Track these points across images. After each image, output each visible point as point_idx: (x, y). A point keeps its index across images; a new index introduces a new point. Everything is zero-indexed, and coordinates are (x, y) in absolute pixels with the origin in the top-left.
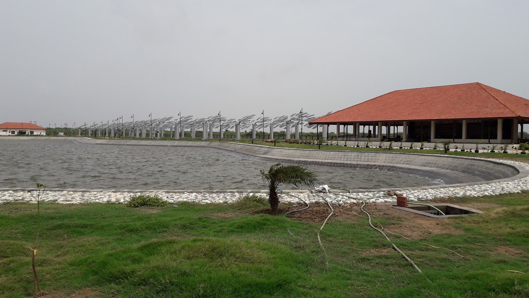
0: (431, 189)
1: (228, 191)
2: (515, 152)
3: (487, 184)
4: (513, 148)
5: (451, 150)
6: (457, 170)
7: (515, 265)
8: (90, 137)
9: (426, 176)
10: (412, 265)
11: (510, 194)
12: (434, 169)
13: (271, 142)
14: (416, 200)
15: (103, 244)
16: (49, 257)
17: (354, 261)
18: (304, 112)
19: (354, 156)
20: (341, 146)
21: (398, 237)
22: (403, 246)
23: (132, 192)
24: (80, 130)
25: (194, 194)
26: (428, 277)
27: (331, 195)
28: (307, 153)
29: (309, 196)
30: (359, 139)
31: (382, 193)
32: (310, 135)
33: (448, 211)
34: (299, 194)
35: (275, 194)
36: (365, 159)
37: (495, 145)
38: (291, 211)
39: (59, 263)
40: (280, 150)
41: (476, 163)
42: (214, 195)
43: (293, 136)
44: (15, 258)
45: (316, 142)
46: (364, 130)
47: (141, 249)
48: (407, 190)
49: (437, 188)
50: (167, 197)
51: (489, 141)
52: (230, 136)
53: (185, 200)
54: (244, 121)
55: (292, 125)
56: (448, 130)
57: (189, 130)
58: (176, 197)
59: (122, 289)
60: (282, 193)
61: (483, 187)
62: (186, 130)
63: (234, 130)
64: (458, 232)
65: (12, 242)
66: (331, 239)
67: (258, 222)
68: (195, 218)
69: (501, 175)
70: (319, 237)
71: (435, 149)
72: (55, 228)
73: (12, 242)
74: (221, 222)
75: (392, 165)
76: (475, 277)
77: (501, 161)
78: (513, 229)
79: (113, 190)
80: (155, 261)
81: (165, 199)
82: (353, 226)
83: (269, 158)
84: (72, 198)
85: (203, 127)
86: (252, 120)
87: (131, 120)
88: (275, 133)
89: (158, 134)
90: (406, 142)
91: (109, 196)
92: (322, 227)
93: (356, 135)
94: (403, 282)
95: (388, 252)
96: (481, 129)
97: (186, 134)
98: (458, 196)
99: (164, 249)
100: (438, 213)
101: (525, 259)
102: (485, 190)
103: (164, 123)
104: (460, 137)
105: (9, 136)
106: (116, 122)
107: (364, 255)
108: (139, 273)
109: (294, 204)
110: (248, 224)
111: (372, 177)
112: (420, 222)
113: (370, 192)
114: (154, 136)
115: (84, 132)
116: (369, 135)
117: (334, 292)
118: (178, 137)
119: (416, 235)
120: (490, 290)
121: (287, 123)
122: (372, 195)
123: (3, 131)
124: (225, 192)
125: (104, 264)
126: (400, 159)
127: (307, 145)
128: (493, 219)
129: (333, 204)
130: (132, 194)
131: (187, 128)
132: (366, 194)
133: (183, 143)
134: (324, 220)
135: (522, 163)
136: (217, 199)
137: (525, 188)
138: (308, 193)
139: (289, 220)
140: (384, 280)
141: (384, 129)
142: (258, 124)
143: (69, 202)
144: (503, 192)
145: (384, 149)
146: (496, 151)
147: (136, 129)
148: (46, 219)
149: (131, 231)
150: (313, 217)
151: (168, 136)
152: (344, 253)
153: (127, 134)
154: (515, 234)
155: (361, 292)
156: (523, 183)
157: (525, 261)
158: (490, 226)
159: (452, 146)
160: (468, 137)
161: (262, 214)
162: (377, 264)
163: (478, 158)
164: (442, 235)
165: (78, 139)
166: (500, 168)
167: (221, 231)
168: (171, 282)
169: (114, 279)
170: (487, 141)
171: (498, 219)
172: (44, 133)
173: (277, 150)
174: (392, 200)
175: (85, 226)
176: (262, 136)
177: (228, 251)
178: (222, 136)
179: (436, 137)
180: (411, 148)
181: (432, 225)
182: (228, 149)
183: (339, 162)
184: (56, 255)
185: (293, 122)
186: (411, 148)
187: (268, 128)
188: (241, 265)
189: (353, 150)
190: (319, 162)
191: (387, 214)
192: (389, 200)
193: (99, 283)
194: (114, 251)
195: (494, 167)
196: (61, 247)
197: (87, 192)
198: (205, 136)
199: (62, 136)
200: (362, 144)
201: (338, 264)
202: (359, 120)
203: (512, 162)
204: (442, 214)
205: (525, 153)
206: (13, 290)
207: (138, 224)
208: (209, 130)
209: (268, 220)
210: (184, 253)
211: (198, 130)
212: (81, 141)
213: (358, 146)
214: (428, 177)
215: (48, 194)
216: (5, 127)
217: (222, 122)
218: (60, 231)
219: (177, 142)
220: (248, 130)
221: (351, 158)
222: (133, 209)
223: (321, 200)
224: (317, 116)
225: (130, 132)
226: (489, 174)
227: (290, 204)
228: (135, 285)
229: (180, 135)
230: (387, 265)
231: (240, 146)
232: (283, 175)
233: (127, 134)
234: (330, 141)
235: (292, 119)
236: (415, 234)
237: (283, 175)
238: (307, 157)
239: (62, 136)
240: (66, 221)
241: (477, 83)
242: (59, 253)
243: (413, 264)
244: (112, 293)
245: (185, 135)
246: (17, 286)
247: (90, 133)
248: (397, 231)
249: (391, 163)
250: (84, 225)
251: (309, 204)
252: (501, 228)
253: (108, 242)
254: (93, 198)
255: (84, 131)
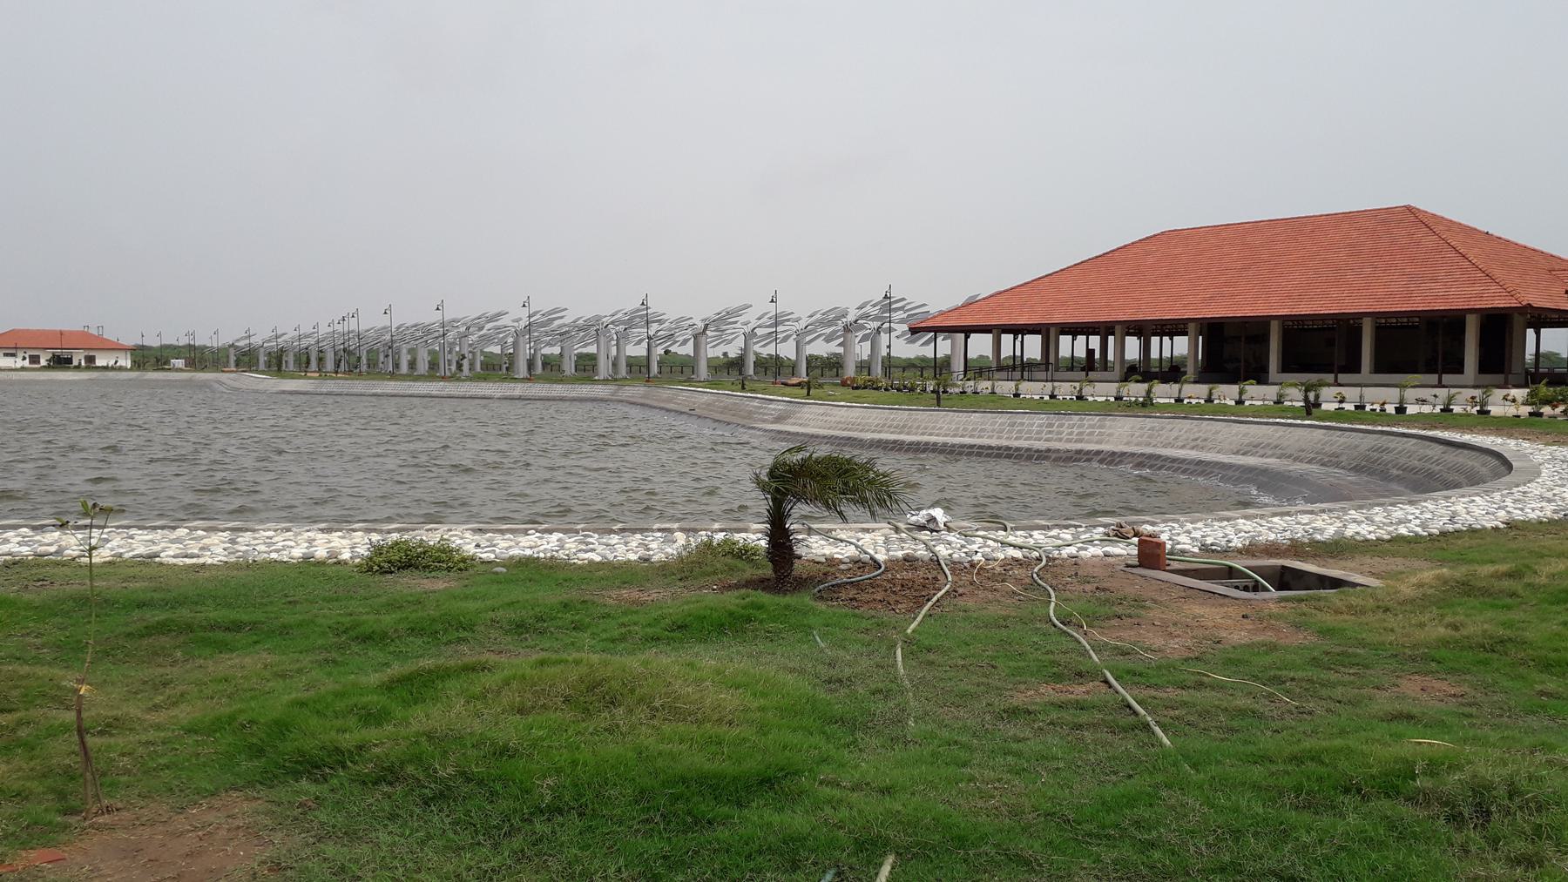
0: (1246, 517)
1: (656, 526)
2: (1511, 411)
3: (1411, 503)
4: (1505, 398)
5: (1324, 406)
6: (1337, 465)
7: (1436, 725)
8: (262, 372)
9: (1248, 481)
10: (1147, 727)
11: (1472, 531)
12: (1272, 462)
13: (799, 385)
14: (1196, 550)
15: (283, 676)
16: (133, 710)
17: (988, 717)
18: (896, 295)
19: (1040, 426)
20: (1003, 398)
21: (1125, 654)
22: (1131, 676)
23: (375, 530)
24: (232, 351)
25: (555, 536)
26: (1186, 757)
27: (951, 537)
28: (900, 416)
29: (887, 540)
30: (1057, 375)
31: (1101, 529)
32: (918, 363)
33: (1285, 579)
34: (860, 535)
35: (786, 533)
36: (1070, 433)
37: (1453, 391)
38: (829, 581)
39: (158, 727)
40: (822, 409)
41: (1394, 443)
42: (614, 539)
43: (864, 366)
44: (34, 713)
45: (930, 387)
46: (1067, 346)
47: (389, 687)
48: (1174, 520)
49: (1262, 517)
50: (478, 546)
51: (1440, 380)
52: (678, 370)
53: (528, 552)
54: (720, 322)
55: (860, 334)
56: (1320, 346)
57: (556, 350)
58: (503, 544)
59: (326, 794)
60: (810, 531)
61: (1398, 513)
62: (547, 351)
63: (688, 350)
64: (1300, 639)
65: (25, 669)
66: (931, 657)
67: (731, 614)
68: (550, 603)
69: (1462, 479)
70: (899, 652)
71: (1278, 402)
72: (151, 630)
73: (25, 669)
74: (625, 613)
75: (1149, 450)
76: (1316, 758)
77: (1467, 438)
78: (1456, 628)
79: (323, 526)
80: (423, 718)
81: (470, 549)
82: (1001, 623)
83: (789, 433)
84: (202, 549)
85: (597, 341)
86: (741, 319)
87: (383, 321)
88: (811, 360)
89: (465, 363)
90: (1195, 382)
91: (311, 541)
92: (913, 626)
93: (1048, 365)
94: (1115, 773)
95: (1088, 692)
96: (1420, 344)
97: (548, 363)
98: (1318, 537)
99: (453, 686)
100: (1256, 588)
101: (1474, 710)
102: (1400, 522)
103: (481, 329)
104: (1355, 367)
105: (23, 369)
106: (339, 328)
107: (1018, 700)
108: (377, 750)
109: (841, 562)
110: (702, 618)
111: (1082, 481)
112: (1198, 610)
113: (1067, 527)
114: (454, 368)
115: (246, 359)
116: (1089, 365)
117: (917, 798)
118: (522, 371)
119: (1175, 647)
120: (1347, 791)
121: (847, 329)
122: (1069, 537)
123: (6, 355)
124: (647, 530)
125: (281, 728)
126: (1175, 434)
127: (903, 396)
128: (1404, 602)
129: (954, 563)
130: (375, 537)
131: (548, 344)
132: (1054, 532)
133: (538, 389)
134: (921, 606)
135: (1526, 444)
136: (621, 549)
137: (1518, 515)
138: (887, 531)
139: (822, 606)
140: (1061, 765)
141: (1133, 347)
142: (759, 332)
143: (194, 561)
144: (1450, 528)
145: (1130, 405)
146: (1457, 409)
147: (399, 348)
148: (125, 607)
149: (366, 639)
150: (892, 598)
151: (494, 368)
152: (963, 695)
153: (372, 364)
154: (1456, 642)
155: (993, 797)
156: (1515, 501)
157: (1470, 716)
158: (1391, 621)
159: (1327, 393)
160: (1379, 368)
161: (743, 591)
162: (1052, 723)
163: (1401, 430)
164: (1251, 646)
165: (230, 378)
166: (1462, 458)
167: (623, 638)
168: (463, 774)
169: (311, 766)
170: (1433, 378)
171: (1421, 602)
172: (125, 362)
173: (815, 409)
174: (1126, 550)
175: (236, 627)
176: (773, 368)
177: (632, 691)
178: (655, 369)
179: (1286, 368)
180: (1209, 400)
181: (1226, 620)
182: (671, 406)
183: (994, 442)
184: (150, 704)
185: (863, 327)
186: (1209, 400)
187: (791, 343)
188: (667, 728)
189: (1037, 407)
190: (935, 444)
191: (1104, 590)
192: (1119, 549)
193: (268, 779)
194: (312, 693)
195: (1446, 457)
196: (165, 685)
197: (247, 530)
198: (604, 369)
199: (181, 370)
200: (1066, 390)
201: (942, 725)
202: (1058, 318)
203: (1499, 440)
204: (1267, 590)
205: (1541, 415)
206: (26, 798)
207: (388, 619)
208: (614, 351)
209: (760, 607)
210: (509, 697)
211: (584, 350)
212: (236, 385)
213: (1052, 396)
214: (1280, 487)
215: (132, 537)
216: (10, 344)
217: (654, 327)
218: (164, 640)
219: (520, 385)
220: (733, 351)
221: (1031, 431)
222: (377, 578)
223: (922, 552)
224: (933, 309)
225: (382, 358)
226: (1430, 475)
227: (831, 562)
228: (364, 783)
229: (531, 364)
230: (1079, 727)
231: (706, 397)
232: (805, 481)
233: (372, 364)
234: (972, 383)
235: (861, 317)
236: (1173, 643)
237: (805, 481)
238: (902, 429)
239: (181, 370)
240: (184, 613)
241: (1409, 209)
242: (159, 699)
243: (1152, 724)
244: (301, 805)
245: (545, 365)
246: (34, 786)
247: (262, 359)
248: (1124, 636)
249: (1148, 444)
250: (233, 622)
251: (885, 562)
252: (1422, 625)
253: (300, 671)
254: (263, 548)
255: (245, 354)
